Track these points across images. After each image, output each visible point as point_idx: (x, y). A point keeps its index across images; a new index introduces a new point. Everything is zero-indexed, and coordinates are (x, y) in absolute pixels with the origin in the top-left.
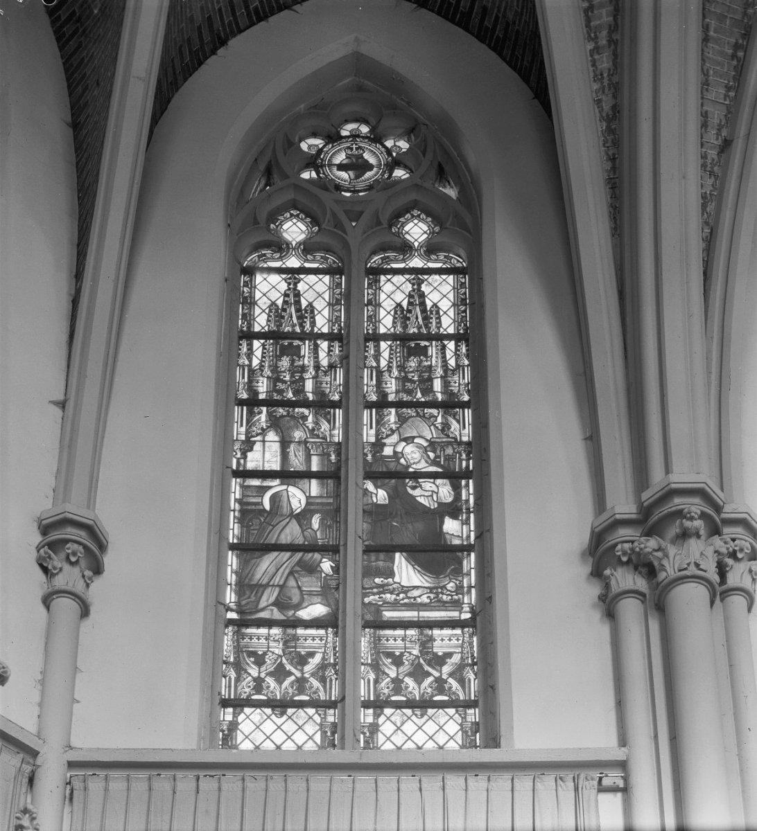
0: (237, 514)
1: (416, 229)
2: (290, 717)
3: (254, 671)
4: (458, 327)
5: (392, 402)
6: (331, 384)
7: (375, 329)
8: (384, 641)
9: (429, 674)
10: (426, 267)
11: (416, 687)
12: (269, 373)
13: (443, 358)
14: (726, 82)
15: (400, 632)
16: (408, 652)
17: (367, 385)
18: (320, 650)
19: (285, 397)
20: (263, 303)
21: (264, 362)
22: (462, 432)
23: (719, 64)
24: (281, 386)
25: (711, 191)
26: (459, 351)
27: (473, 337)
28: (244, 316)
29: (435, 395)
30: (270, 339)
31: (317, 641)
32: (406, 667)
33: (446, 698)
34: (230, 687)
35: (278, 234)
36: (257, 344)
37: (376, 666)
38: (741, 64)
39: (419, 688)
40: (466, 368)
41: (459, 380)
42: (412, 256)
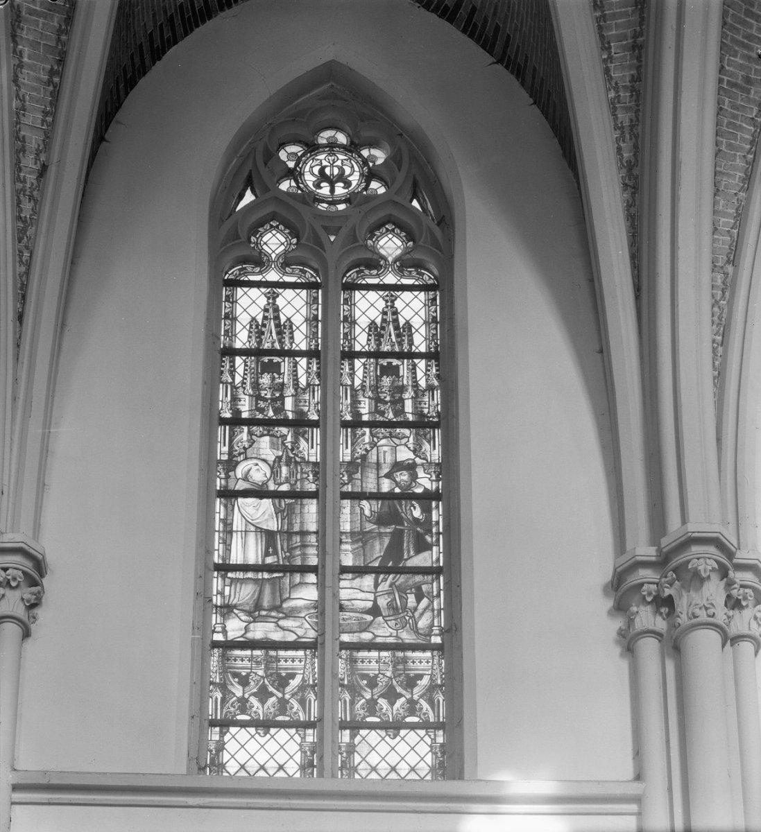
0: (221, 535)
1: (274, 240)
2: (403, 739)
3: (238, 691)
4: (429, 346)
5: (245, 419)
6: (309, 403)
7: (351, 347)
8: (360, 665)
10: (281, 280)
11: (260, 707)
12: (251, 392)
13: (413, 378)
14: (43, 107)
15: (374, 654)
16: (382, 674)
17: (222, 401)
18: (299, 672)
19: (387, 418)
20: (363, 322)
21: (246, 379)
22: (432, 452)
23: (34, 89)
24: (262, 404)
25: (31, 215)
26: (310, 368)
27: (444, 356)
28: (346, 335)
29: (286, 414)
30: (251, 356)
31: (424, 664)
33: (378, 720)
34: (216, 709)
35: (374, 250)
36: (239, 361)
37: (223, 687)
38: (58, 89)
39: (263, 707)
40: (316, 388)
41: (429, 401)
42: (267, 271)
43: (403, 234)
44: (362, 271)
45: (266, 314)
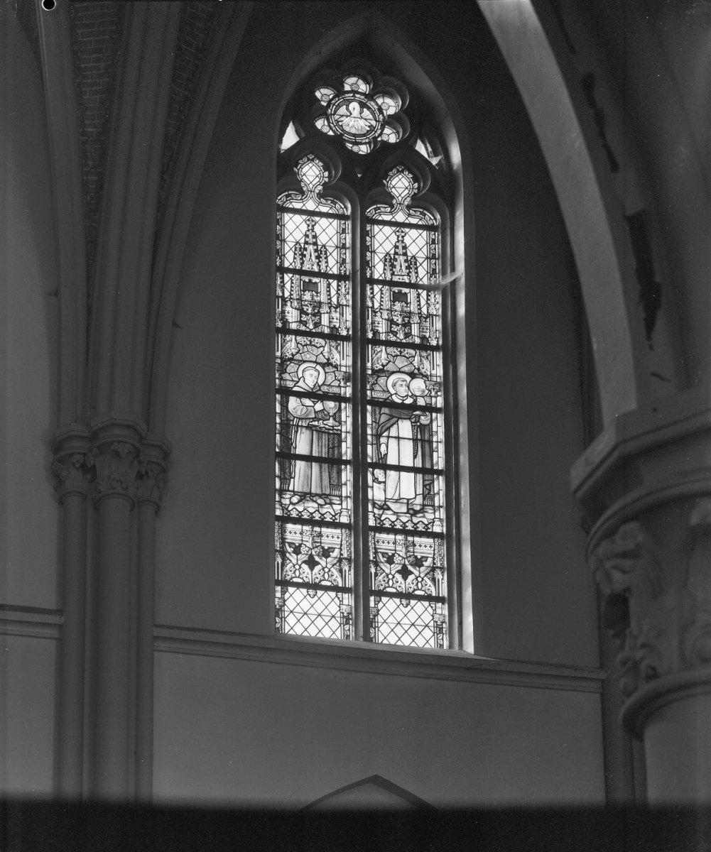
9: (412, 573)
20: (381, 253)
32: (303, 557)
36: (287, 277)
43: (410, 176)
44: (379, 208)
45: (307, 240)
